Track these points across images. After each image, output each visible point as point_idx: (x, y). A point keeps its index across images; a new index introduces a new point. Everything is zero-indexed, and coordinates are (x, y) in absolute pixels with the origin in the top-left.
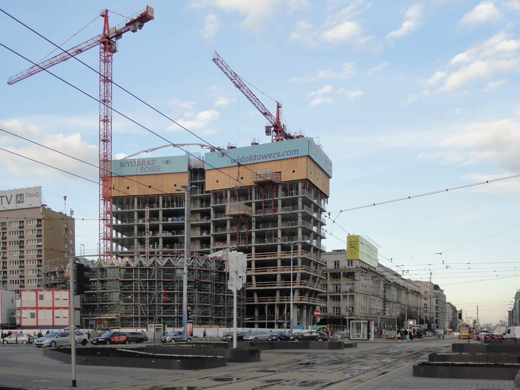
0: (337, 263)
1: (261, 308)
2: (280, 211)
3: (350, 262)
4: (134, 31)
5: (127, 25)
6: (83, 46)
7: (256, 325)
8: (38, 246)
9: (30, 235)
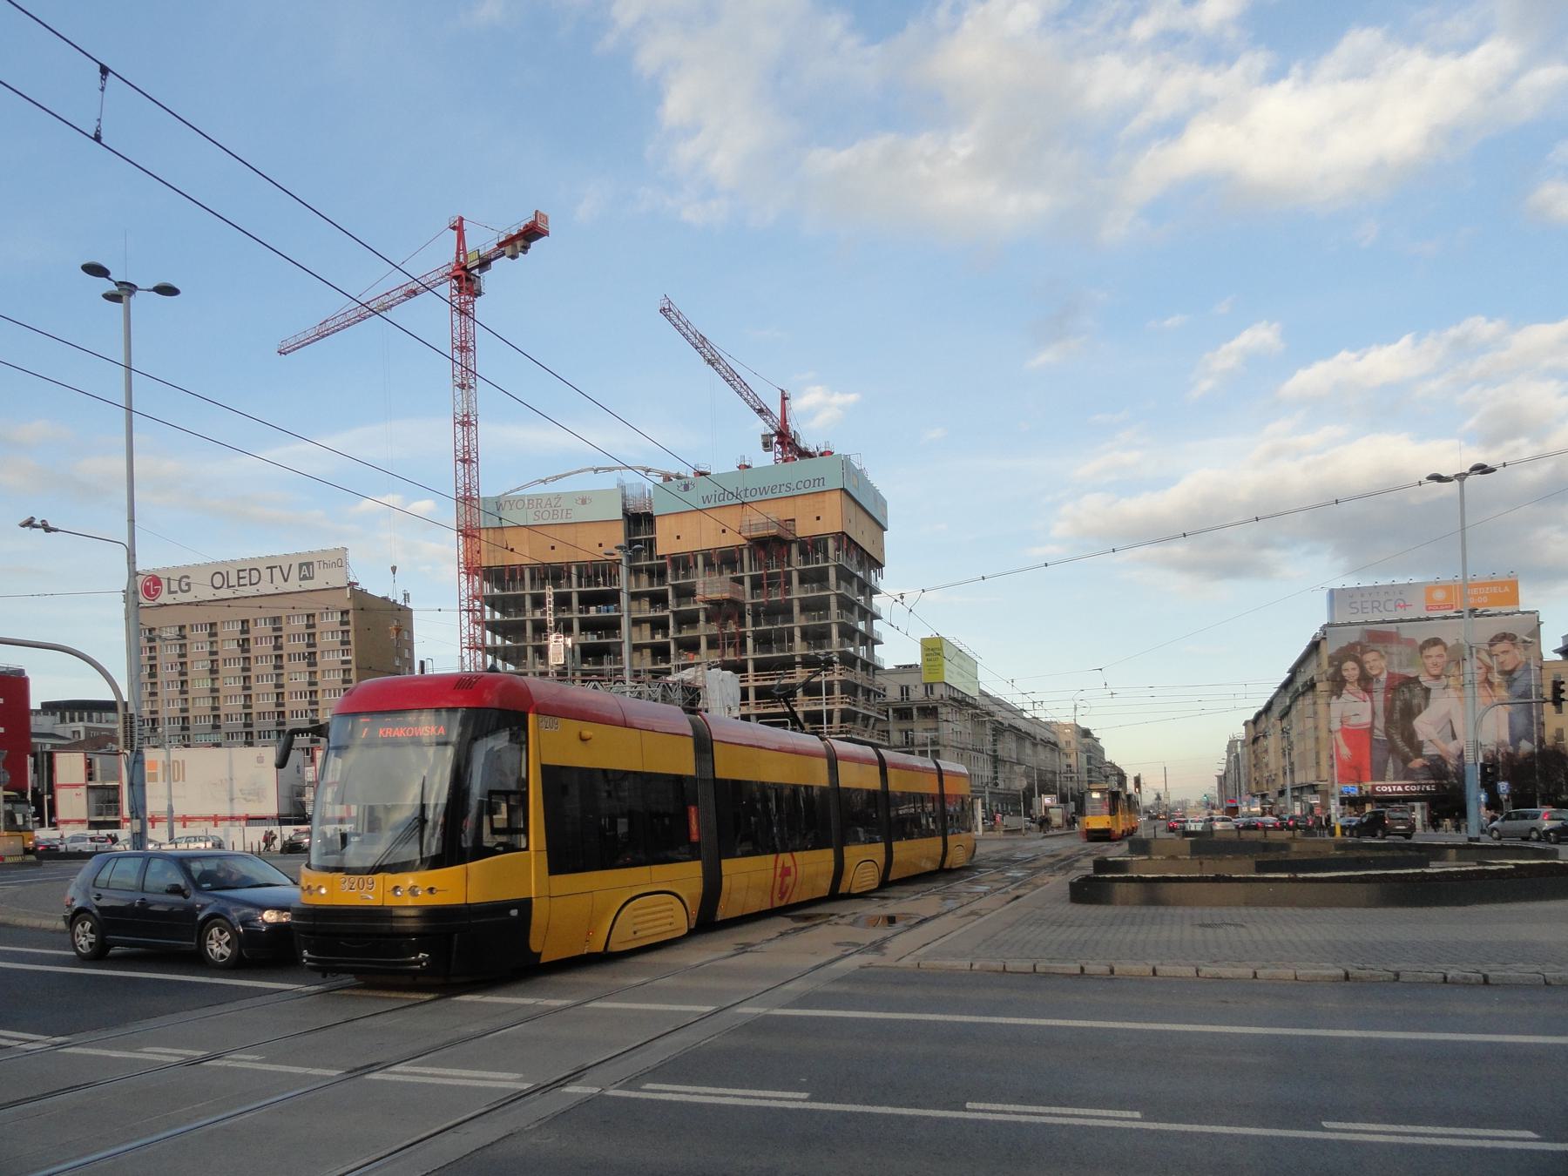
0: (905, 690)
3: (929, 687)
4: (513, 257)
5: (500, 245)
8: (344, 662)
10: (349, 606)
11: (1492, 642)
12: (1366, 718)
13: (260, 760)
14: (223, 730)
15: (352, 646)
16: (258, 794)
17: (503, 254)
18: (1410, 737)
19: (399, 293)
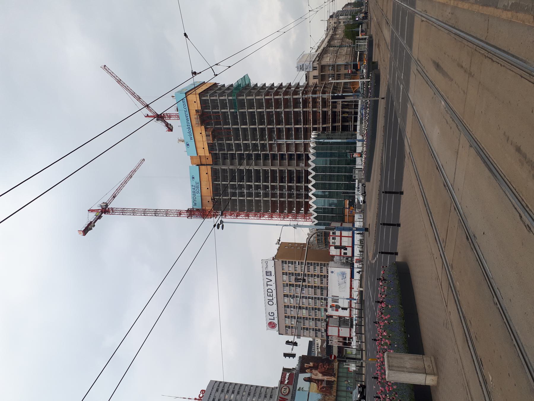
0: (315, 77)
1: (344, 120)
2: (282, 110)
3: (314, 68)
7: (355, 124)
8: (299, 264)
10: (280, 261)
13: (332, 272)
14: (320, 307)
15: (294, 261)
16: (343, 274)
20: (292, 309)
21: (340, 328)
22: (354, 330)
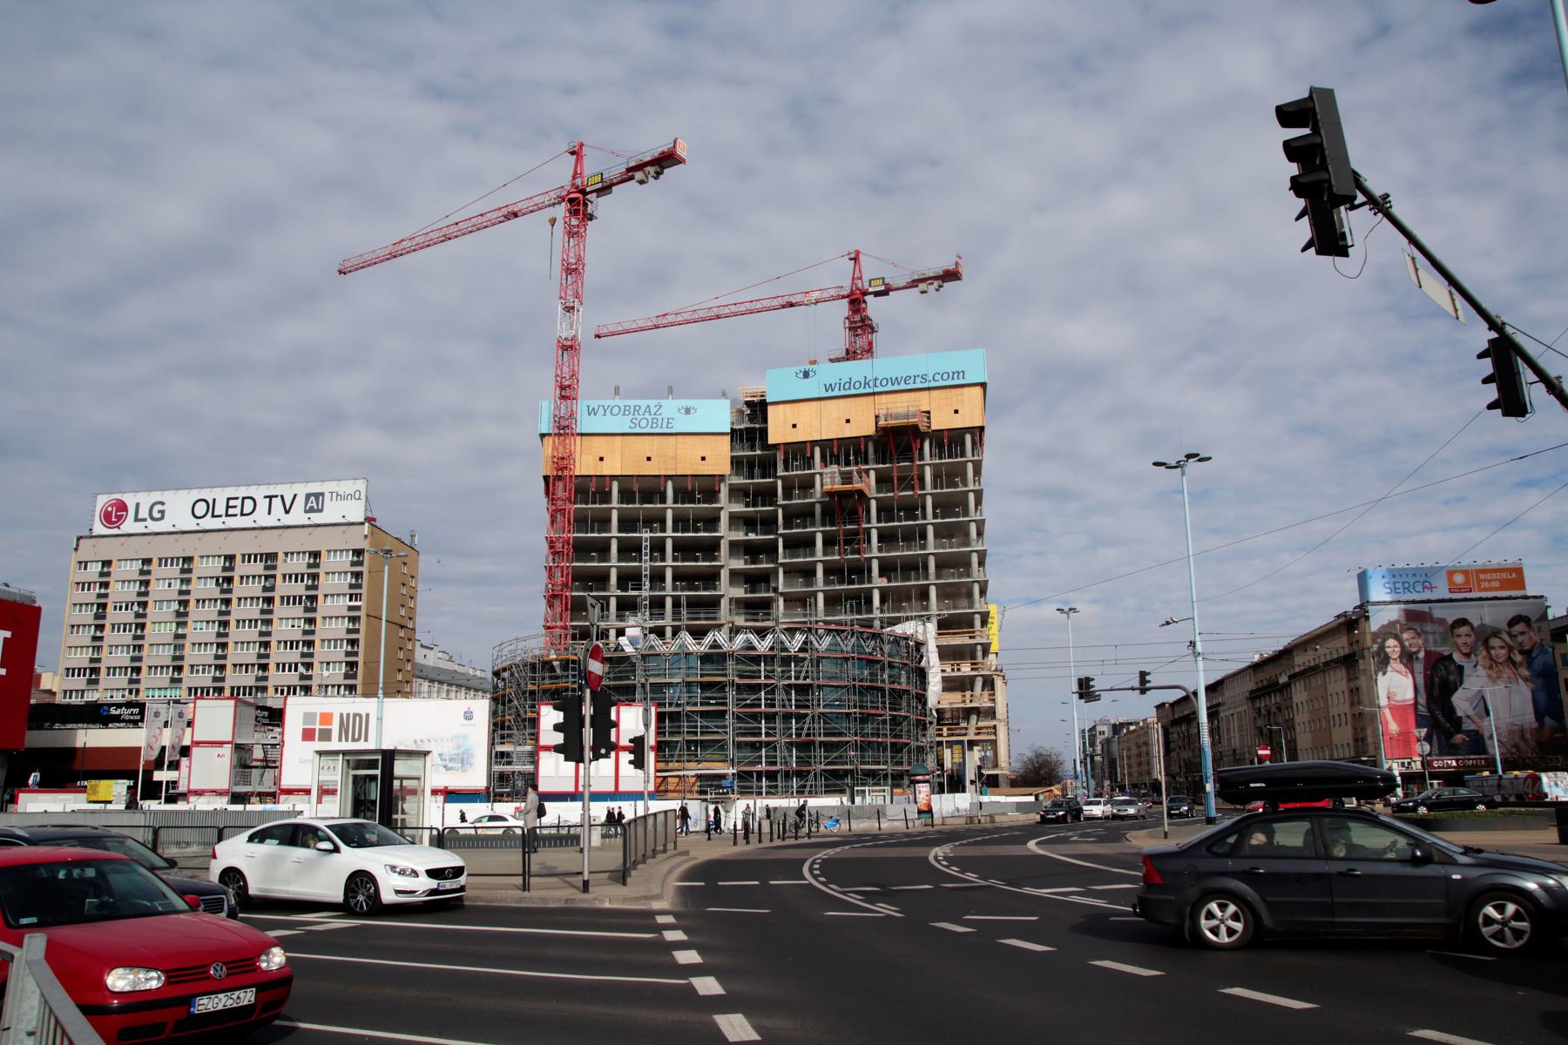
4: (641, 182)
5: (629, 170)
6: (520, 206)
8: (351, 608)
9: (334, 582)
11: (1511, 623)
12: (1410, 695)
13: (468, 716)
14: (186, 684)
16: (463, 760)
17: (632, 178)
18: (1450, 710)
19: (495, 215)
20: (177, 585)
21: (227, 750)
22: (222, 803)
